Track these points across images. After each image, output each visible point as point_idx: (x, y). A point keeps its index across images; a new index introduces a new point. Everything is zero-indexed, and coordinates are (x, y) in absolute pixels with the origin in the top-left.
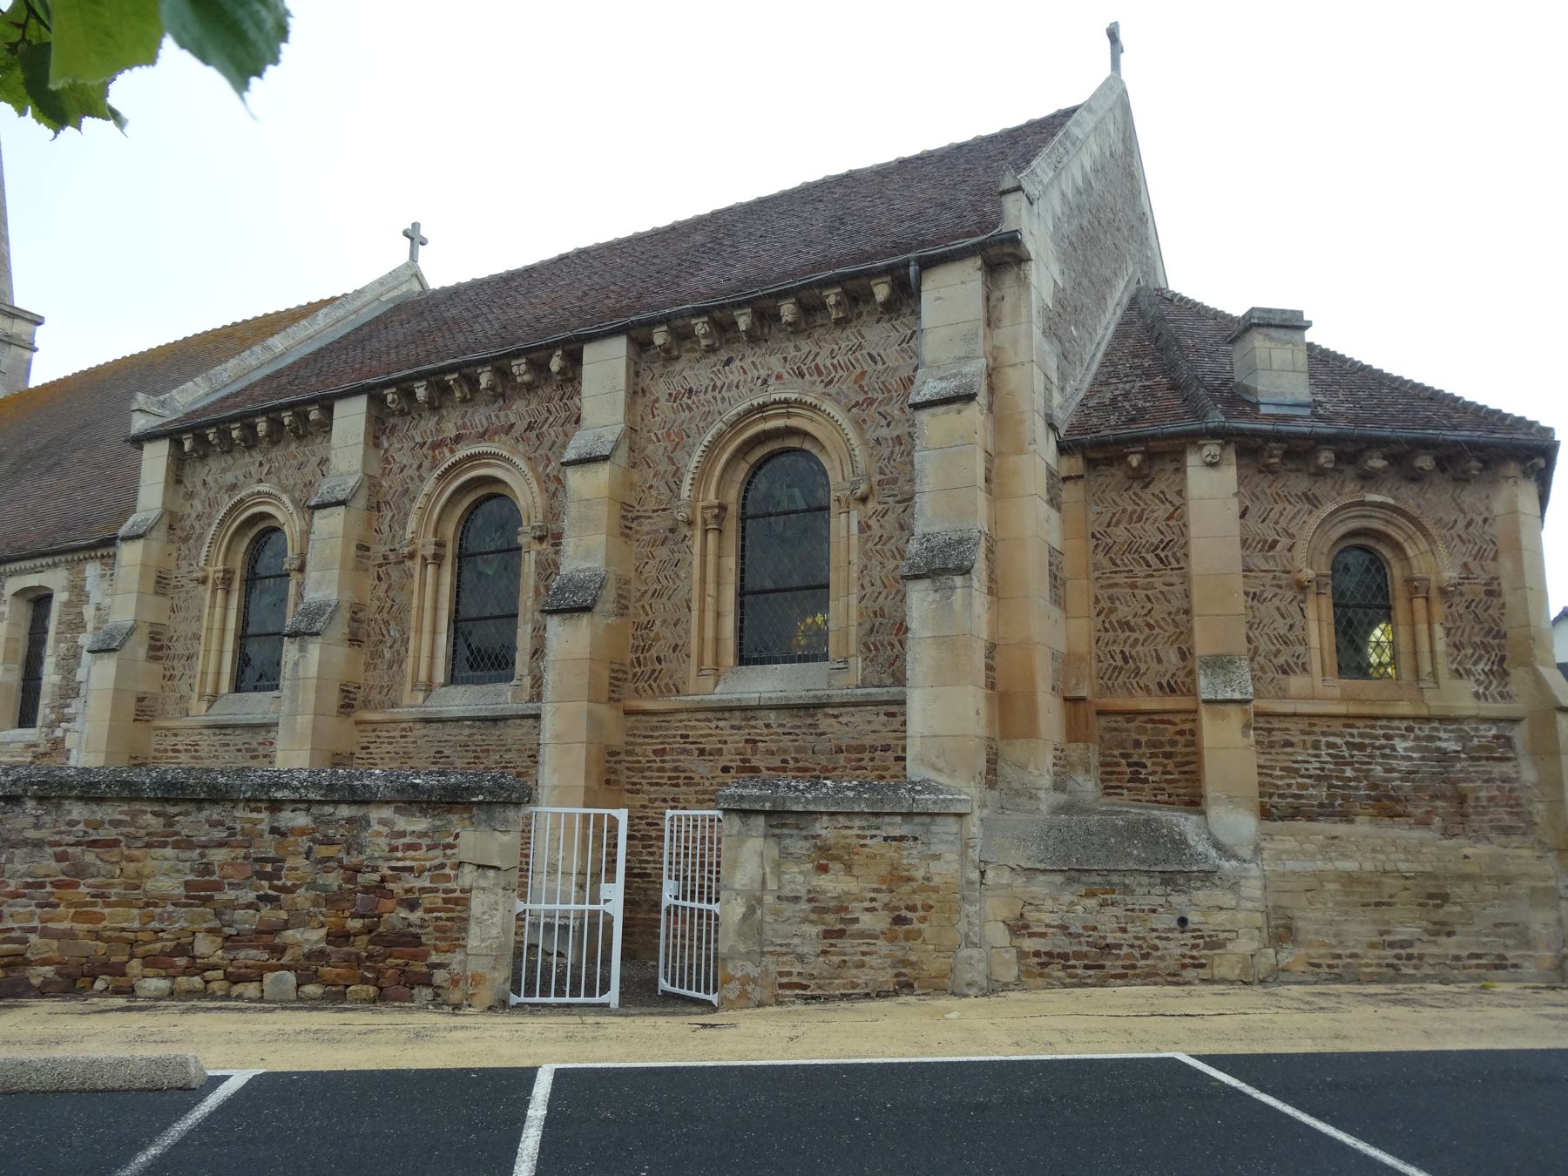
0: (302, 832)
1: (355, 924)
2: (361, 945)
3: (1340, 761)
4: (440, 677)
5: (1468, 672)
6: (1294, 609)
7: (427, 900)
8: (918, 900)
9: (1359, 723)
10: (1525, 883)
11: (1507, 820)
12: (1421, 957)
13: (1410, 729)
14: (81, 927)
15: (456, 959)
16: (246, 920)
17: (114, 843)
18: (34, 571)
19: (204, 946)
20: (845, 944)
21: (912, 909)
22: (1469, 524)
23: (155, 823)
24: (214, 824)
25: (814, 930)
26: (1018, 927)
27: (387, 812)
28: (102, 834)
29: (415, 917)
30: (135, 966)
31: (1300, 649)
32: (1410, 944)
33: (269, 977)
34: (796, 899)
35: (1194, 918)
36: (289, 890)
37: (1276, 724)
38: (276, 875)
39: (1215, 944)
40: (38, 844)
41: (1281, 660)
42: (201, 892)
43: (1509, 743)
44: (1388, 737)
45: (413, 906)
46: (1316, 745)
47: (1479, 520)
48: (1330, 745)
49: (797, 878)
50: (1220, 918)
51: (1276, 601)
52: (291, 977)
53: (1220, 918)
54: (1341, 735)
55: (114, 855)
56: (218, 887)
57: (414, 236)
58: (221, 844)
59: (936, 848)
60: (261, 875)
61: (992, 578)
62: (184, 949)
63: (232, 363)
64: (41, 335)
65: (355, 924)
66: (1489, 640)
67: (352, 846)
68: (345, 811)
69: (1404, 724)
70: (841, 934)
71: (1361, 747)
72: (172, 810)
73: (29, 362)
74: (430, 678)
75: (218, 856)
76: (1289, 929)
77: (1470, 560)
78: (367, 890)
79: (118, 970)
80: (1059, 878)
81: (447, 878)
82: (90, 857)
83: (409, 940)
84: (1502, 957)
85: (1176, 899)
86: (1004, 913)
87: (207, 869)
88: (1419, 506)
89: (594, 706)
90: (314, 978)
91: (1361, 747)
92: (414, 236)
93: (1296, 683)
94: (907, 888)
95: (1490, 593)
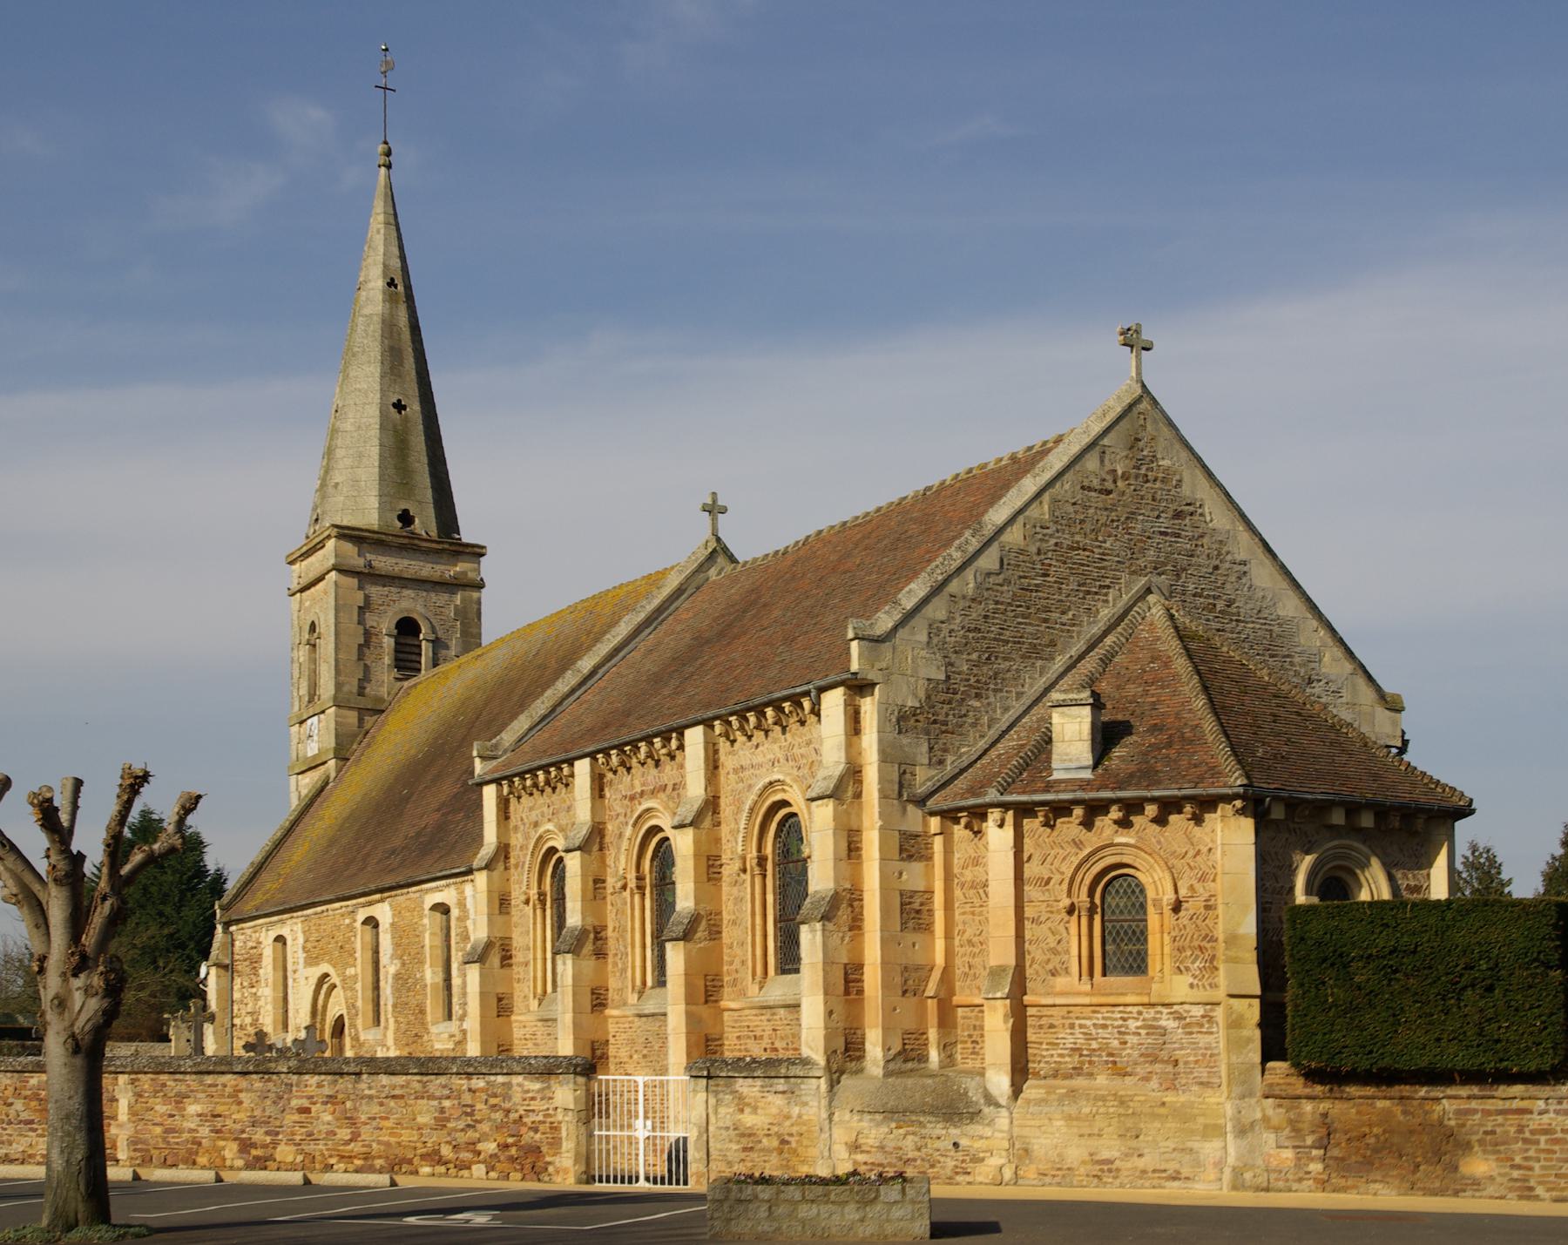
0: (482, 1090)
1: (510, 1140)
2: (513, 1151)
3: (1089, 1037)
4: (649, 983)
5: (1187, 969)
6: (1061, 928)
7: (541, 1128)
8: (794, 1130)
9: (1104, 1009)
10: (1201, 1120)
11: (1204, 1077)
12: (1118, 1170)
13: (1140, 1013)
14: (393, 1140)
15: (557, 1159)
16: (462, 1138)
17: (402, 1097)
18: (437, 889)
19: (446, 1151)
20: (754, 1155)
21: (791, 1135)
22: (1198, 853)
23: (417, 1086)
24: (444, 1087)
25: (735, 1147)
26: (855, 1147)
27: (520, 1079)
28: (397, 1092)
29: (538, 1136)
30: (416, 1161)
31: (1065, 958)
32: (1111, 1162)
33: (474, 1167)
34: (727, 1128)
35: (963, 1142)
36: (479, 1122)
37: (1045, 1011)
38: (471, 1114)
39: (977, 1160)
40: (370, 1097)
41: (1050, 966)
42: (441, 1122)
43: (1211, 1019)
44: (1124, 1019)
45: (536, 1131)
46: (1072, 1026)
47: (1205, 850)
48: (1081, 1026)
49: (726, 1113)
50: (978, 1144)
51: (1049, 924)
52: (482, 1167)
53: (978, 1144)
54: (1090, 1018)
55: (402, 1103)
56: (448, 1120)
57: (714, 509)
58: (448, 1098)
59: (804, 1099)
60: (467, 1114)
61: (450, 996)
62: (437, 1152)
63: (549, 693)
64: (488, 568)
65: (510, 1140)
66: (1204, 944)
67: (507, 1097)
68: (500, 1079)
69: (1135, 1009)
70: (752, 1149)
71: (1105, 1027)
72: (425, 1078)
73: (479, 602)
74: (644, 983)
75: (447, 1103)
76: (1026, 1150)
77: (1194, 882)
78: (515, 1122)
79: (410, 1162)
80: (879, 1117)
81: (549, 1116)
82: (392, 1104)
83: (536, 1150)
84: (1178, 1172)
85: (953, 1131)
86: (846, 1139)
87: (442, 1110)
88: (1159, 842)
89: (693, 1008)
90: (493, 1168)
91: (1105, 1027)
92: (714, 509)
93: (1061, 982)
94: (788, 1123)
95: (1207, 908)
